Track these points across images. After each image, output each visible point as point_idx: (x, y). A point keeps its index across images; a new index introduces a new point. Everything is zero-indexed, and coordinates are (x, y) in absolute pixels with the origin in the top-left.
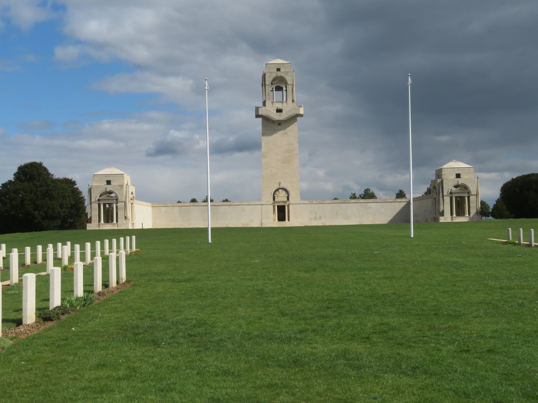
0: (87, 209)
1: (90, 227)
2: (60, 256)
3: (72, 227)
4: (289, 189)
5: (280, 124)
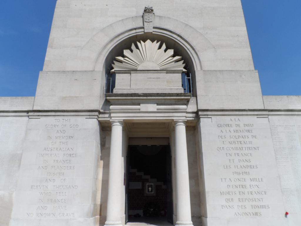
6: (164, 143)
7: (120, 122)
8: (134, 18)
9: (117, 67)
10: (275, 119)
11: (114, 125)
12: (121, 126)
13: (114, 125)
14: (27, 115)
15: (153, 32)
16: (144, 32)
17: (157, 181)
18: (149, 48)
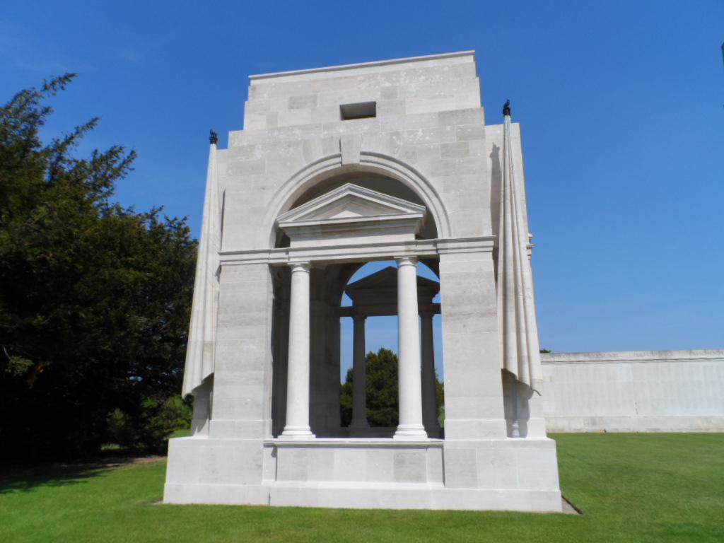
1: (206, 467)
2: (293, 245)
7: (304, 266)
11: (401, 266)
12: (305, 273)
13: (401, 266)
14: (287, 256)
15: (361, 161)
16: (341, 163)
17: (241, 128)
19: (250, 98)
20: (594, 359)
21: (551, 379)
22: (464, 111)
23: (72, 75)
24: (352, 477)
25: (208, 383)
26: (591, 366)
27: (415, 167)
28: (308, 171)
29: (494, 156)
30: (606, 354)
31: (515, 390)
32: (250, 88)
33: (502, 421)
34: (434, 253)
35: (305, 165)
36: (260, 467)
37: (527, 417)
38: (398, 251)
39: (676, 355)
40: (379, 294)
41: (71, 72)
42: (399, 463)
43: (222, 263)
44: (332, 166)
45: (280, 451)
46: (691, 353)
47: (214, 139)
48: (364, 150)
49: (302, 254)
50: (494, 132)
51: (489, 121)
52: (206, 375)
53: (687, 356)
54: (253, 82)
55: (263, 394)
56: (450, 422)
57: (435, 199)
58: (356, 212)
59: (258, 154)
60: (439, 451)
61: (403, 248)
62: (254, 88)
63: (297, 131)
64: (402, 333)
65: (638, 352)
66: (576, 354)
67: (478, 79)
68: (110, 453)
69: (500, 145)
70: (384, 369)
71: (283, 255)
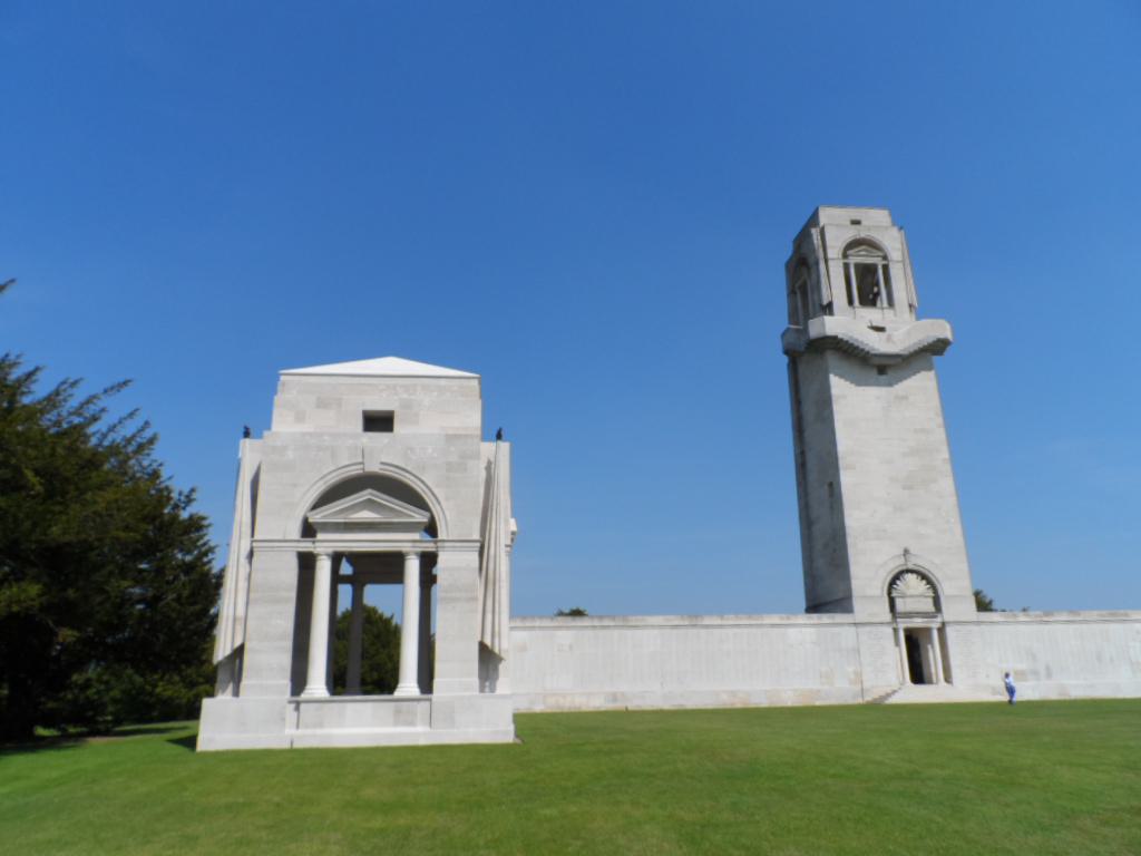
0: (230, 605)
1: (225, 724)
2: (320, 536)
3: (382, 691)
4: (937, 575)
5: (882, 370)
6: (926, 680)
8: (899, 556)
9: (894, 594)
10: (983, 627)
18: (911, 578)
19: (279, 393)
20: (621, 624)
21: (571, 647)
22: (466, 436)
23: (129, 381)
24: (360, 724)
25: (239, 652)
26: (616, 633)
27: (423, 478)
28: (334, 474)
29: (488, 468)
30: (634, 618)
31: (488, 658)
32: (279, 383)
33: (475, 680)
34: (434, 550)
35: (333, 468)
36: (283, 719)
37: (497, 678)
38: (405, 547)
39: (707, 621)
40: (387, 567)
41: (128, 378)
42: (398, 712)
43: (254, 544)
44: (355, 471)
45: (303, 706)
46: (722, 618)
47: (247, 434)
48: (383, 460)
49: (325, 545)
50: (488, 448)
51: (484, 438)
52: (238, 643)
53: (719, 622)
54: (282, 378)
55: (285, 660)
56: (437, 682)
57: (438, 508)
58: (378, 513)
59: (290, 455)
60: (428, 703)
61: (410, 544)
62: (284, 384)
63: (326, 438)
64: (401, 603)
65: (668, 617)
66: (601, 618)
67: (480, 402)
68: (43, 738)
69: (492, 459)
70: (383, 635)
71: (310, 544)
